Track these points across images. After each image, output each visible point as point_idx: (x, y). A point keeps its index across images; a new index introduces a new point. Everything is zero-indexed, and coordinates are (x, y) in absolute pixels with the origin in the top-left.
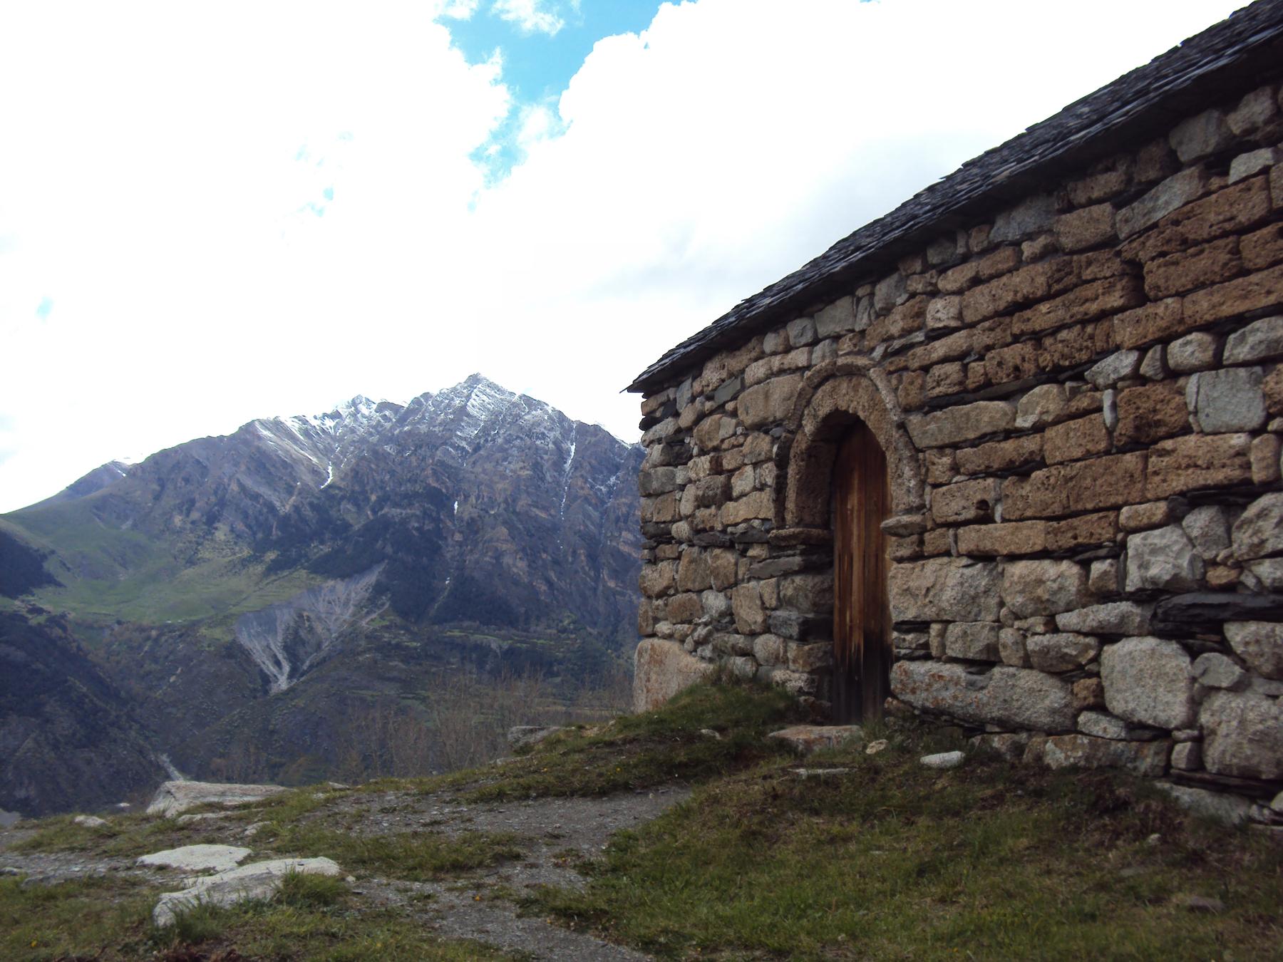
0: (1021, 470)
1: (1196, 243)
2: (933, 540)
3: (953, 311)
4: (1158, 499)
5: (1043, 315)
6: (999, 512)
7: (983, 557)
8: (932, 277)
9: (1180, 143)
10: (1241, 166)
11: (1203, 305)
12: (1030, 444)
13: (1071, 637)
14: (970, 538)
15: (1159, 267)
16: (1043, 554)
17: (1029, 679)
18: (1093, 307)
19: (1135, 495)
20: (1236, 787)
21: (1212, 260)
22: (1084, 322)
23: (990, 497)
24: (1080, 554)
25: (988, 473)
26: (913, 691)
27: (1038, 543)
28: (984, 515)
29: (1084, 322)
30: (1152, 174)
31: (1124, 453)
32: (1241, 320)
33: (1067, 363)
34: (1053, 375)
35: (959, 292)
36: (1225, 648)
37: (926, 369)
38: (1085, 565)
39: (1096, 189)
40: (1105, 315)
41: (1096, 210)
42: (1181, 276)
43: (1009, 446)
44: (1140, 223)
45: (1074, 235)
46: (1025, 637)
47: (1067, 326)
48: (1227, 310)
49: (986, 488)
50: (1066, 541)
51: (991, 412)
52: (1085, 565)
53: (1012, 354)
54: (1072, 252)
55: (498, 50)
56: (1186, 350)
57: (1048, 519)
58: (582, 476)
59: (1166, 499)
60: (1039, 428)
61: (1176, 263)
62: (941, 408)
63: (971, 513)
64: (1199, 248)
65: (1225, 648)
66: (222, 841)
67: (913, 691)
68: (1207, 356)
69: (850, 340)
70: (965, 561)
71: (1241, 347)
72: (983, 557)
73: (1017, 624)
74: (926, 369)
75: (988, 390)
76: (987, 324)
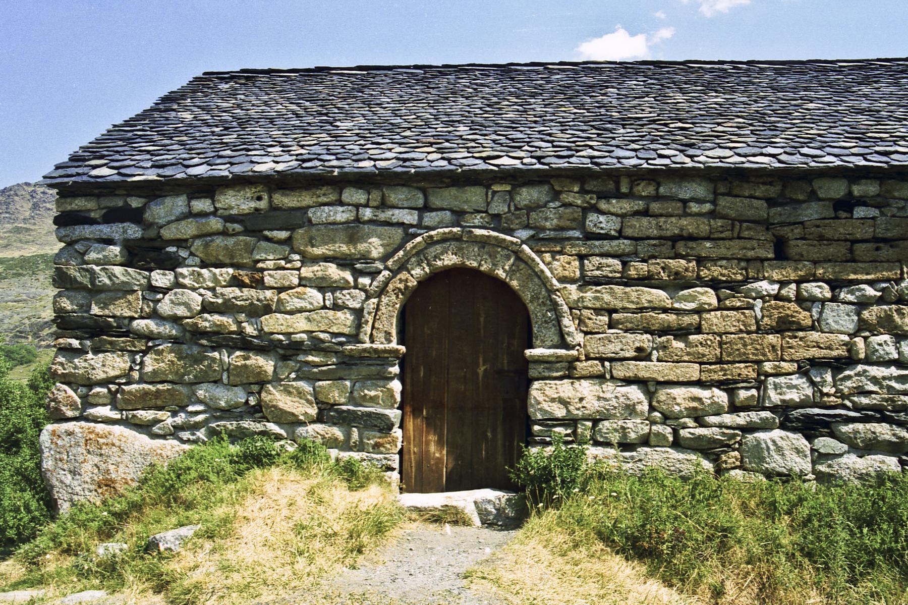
1: (828, 240)
3: (618, 227)
4: (792, 361)
8: (591, 198)
9: (820, 188)
10: (860, 212)
15: (804, 244)
16: (699, 383)
18: (751, 254)
20: (739, 383)
27: (695, 376)
28: (642, 355)
30: (801, 197)
31: (768, 334)
33: (724, 279)
35: (623, 216)
39: (758, 191)
41: (755, 202)
42: (814, 253)
45: (737, 211)
49: (644, 340)
55: (829, 370)
59: (797, 361)
61: (815, 246)
63: (632, 354)
64: (829, 242)
68: (361, 210)
69: (481, 217)
76: (654, 242)
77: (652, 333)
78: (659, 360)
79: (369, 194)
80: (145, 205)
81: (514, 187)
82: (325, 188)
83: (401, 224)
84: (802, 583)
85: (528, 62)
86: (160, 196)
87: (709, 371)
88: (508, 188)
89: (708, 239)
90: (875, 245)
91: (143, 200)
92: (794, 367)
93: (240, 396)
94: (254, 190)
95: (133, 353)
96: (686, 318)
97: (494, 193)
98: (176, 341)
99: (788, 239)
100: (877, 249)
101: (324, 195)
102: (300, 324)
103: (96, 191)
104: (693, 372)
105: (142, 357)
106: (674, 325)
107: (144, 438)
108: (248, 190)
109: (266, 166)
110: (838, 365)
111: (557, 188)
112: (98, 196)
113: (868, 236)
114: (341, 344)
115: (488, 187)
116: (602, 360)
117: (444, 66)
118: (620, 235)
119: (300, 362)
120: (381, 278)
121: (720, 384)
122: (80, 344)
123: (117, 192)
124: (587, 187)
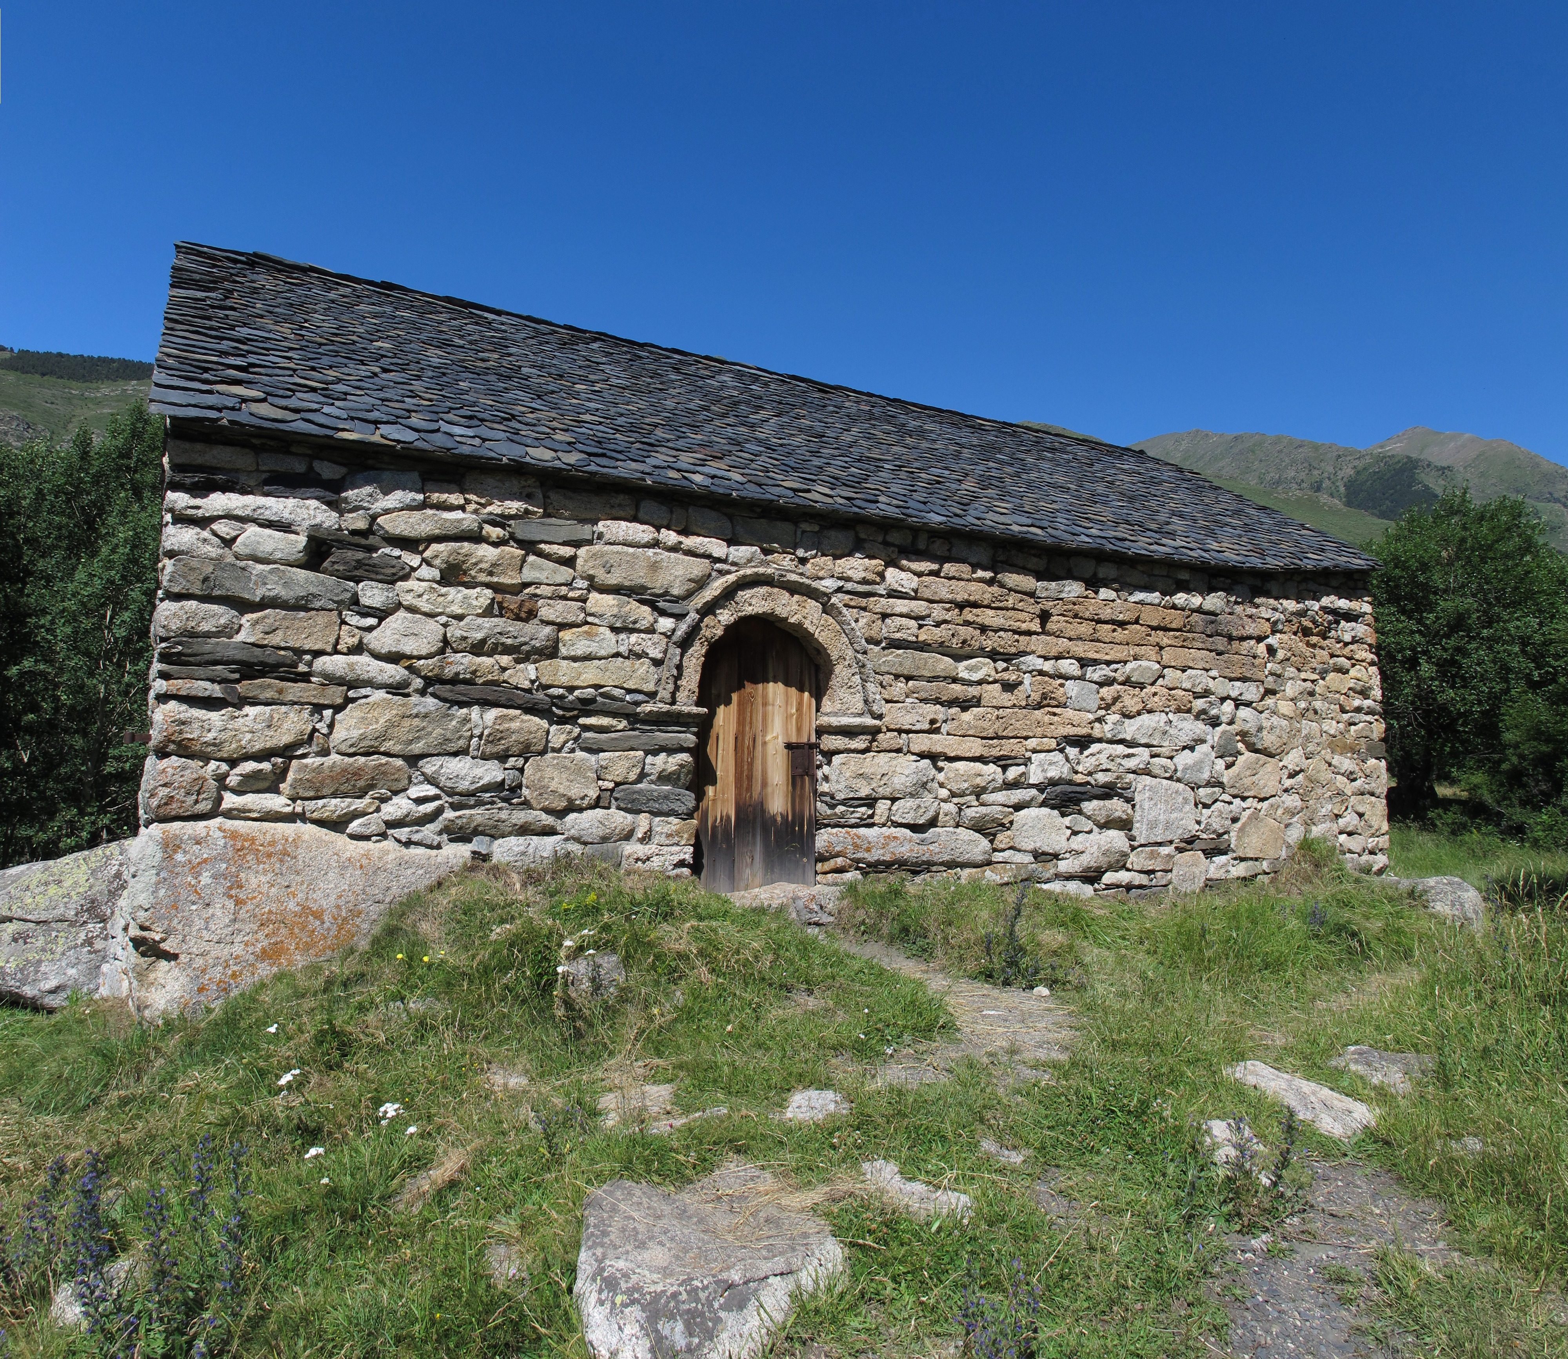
0: (965, 705)
2: (885, 739)
5: (988, 617)
6: (945, 728)
7: (933, 757)
11: (1081, 649)
12: (973, 691)
13: (1000, 808)
14: (921, 743)
16: (981, 759)
17: (965, 834)
19: (1039, 734)
21: (1085, 629)
22: (1015, 632)
23: (941, 717)
24: (1003, 761)
25: (937, 701)
26: (868, 850)
28: (933, 729)
29: (1015, 632)
32: (1095, 662)
34: (994, 655)
36: (1080, 812)
37: (885, 616)
38: (1005, 768)
40: (1029, 633)
43: (957, 687)
44: (1054, 595)
46: (960, 809)
47: (1005, 630)
48: (1092, 655)
49: (938, 712)
50: (995, 752)
51: (945, 664)
52: (1005, 768)
53: (966, 632)
54: (1010, 590)
56: (1069, 666)
57: (983, 738)
58: (1173, 513)
60: (980, 683)
62: (898, 648)
63: (926, 726)
65: (1080, 812)
66: (232, 490)
67: (868, 850)
70: (914, 758)
71: (1096, 673)
72: (933, 757)
73: (955, 800)
74: (885, 616)
75: (943, 649)
77: (942, 704)
78: (948, 734)
79: (672, 512)
80: (343, 478)
81: (823, 528)
82: (621, 497)
83: (708, 556)
84: (155, 1316)
85: (525, 314)
86: (373, 468)
87: (990, 746)
88: (817, 528)
89: (988, 607)
90: (637, 626)
91: (343, 470)
92: (1053, 744)
93: (492, 772)
94: (523, 483)
95: (318, 708)
96: (970, 689)
97: (804, 532)
98: (397, 689)
99: (1051, 615)
100: (1114, 631)
101: (620, 505)
102: (589, 674)
103: (255, 441)
104: (976, 747)
105: (334, 714)
106: (961, 697)
107: (340, 840)
108: (515, 482)
109: (541, 455)
110: (1083, 742)
111: (863, 536)
112: (257, 450)
113: (1108, 617)
114: (637, 704)
115: (796, 524)
116: (900, 731)
117: (255, 255)
118: (915, 596)
119: (581, 726)
120: (688, 619)
121: (996, 760)
122: (224, 691)
123: (294, 449)
124: (890, 539)
